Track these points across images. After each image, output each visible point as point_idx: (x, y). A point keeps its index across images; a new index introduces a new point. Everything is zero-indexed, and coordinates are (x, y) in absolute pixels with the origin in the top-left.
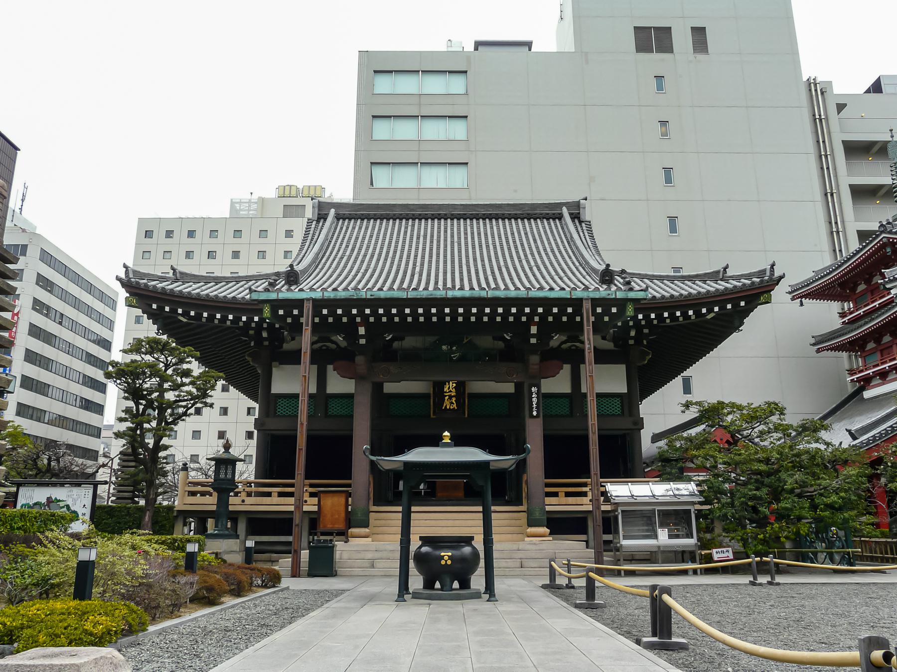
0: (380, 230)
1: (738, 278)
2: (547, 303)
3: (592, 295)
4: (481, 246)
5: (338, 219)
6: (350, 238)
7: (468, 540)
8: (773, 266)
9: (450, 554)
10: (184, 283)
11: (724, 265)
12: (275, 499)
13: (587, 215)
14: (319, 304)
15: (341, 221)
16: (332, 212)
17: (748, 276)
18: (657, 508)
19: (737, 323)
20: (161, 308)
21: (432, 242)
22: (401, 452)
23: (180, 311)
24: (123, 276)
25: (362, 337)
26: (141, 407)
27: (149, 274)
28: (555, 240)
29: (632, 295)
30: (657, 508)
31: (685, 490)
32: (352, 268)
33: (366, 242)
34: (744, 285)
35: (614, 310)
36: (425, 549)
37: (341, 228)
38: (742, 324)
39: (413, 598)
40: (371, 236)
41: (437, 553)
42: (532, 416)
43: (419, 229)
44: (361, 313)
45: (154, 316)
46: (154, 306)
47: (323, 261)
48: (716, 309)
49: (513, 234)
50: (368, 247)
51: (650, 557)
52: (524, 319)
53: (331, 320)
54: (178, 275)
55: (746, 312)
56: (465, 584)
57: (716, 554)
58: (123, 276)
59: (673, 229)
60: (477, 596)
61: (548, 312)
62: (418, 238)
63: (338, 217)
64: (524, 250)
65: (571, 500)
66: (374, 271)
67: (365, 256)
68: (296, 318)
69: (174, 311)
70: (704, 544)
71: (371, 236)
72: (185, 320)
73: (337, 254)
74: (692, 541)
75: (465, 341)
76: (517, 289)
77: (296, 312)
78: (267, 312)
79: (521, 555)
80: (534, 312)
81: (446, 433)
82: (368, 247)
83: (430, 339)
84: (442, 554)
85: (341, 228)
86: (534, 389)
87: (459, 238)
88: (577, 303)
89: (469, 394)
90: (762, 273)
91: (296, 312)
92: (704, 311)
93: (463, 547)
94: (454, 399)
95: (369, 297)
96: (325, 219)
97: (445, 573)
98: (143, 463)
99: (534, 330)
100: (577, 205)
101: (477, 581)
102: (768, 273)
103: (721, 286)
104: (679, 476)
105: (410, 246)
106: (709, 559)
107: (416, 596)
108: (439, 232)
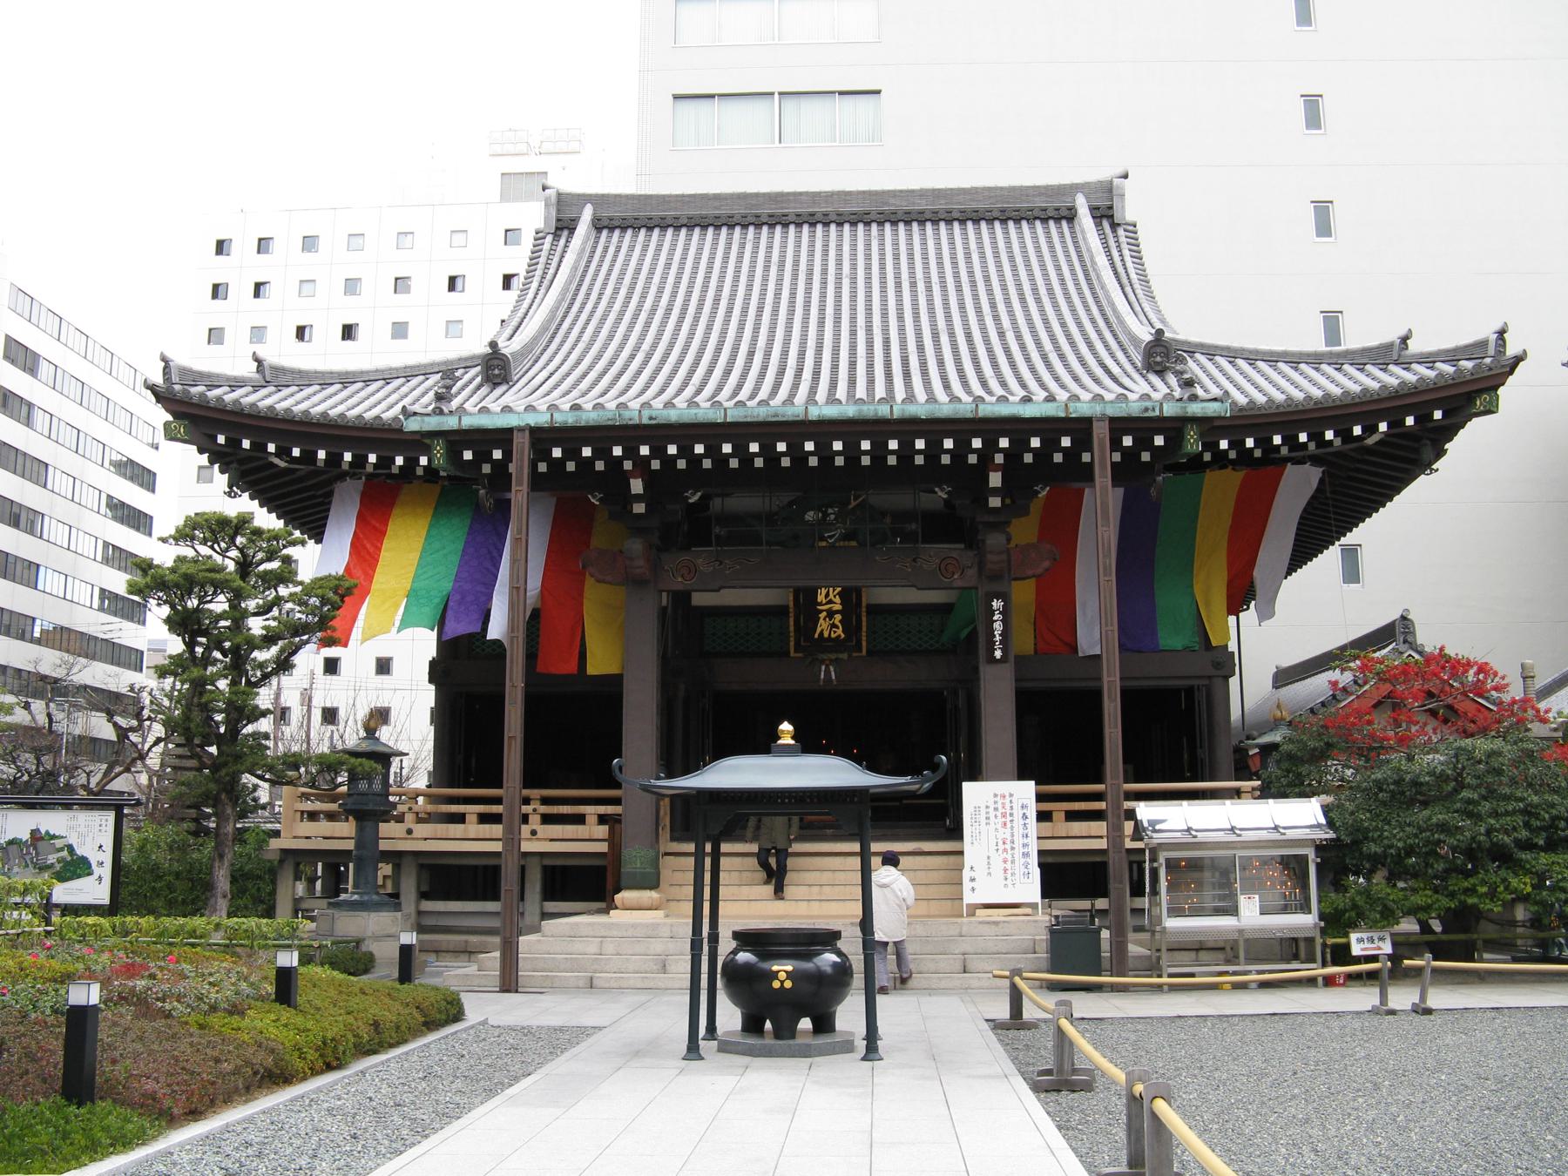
0: (686, 250)
1: (1428, 359)
2: (1019, 427)
3: (1112, 411)
4: (898, 285)
5: (599, 229)
6: (623, 272)
7: (828, 939)
8: (1501, 333)
9: (789, 968)
10: (279, 388)
11: (1403, 332)
12: (472, 828)
13: (1130, 210)
14: (542, 437)
15: (605, 232)
16: (587, 214)
17: (1452, 356)
18: (1240, 853)
19: (1427, 452)
20: (234, 443)
21: (795, 276)
22: (687, 770)
23: (271, 448)
24: (158, 379)
25: (638, 498)
26: (199, 650)
27: (209, 376)
28: (1058, 268)
29: (1195, 409)
30: (1240, 853)
31: (1301, 816)
32: (626, 338)
33: (656, 279)
34: (1441, 375)
35: (1159, 441)
36: (744, 957)
37: (606, 249)
38: (1440, 453)
39: (721, 1050)
40: (668, 266)
41: (765, 965)
42: (992, 660)
43: (770, 247)
44: (631, 452)
45: (222, 458)
46: (221, 439)
47: (566, 325)
48: (1383, 427)
49: (968, 256)
50: (660, 290)
51: (1227, 950)
52: (973, 459)
53: (571, 466)
54: (267, 373)
55: (1449, 430)
56: (824, 1024)
57: (1359, 943)
58: (158, 379)
59: (1324, 227)
60: (847, 1047)
61: (1020, 445)
62: (767, 268)
63: (598, 226)
64: (990, 292)
65: (1078, 827)
66: (671, 345)
67: (653, 311)
68: (501, 468)
69: (259, 447)
70: (1336, 922)
71: (668, 266)
72: (282, 464)
73: (595, 307)
74: (1306, 921)
75: (853, 504)
76: (954, 399)
77: (497, 454)
78: (439, 450)
79: (966, 946)
80: (991, 445)
81: (786, 727)
82: (660, 290)
83: (785, 497)
84: (775, 968)
85: (606, 249)
86: (997, 604)
87: (854, 267)
88: (1080, 427)
89: (868, 606)
90: (1476, 349)
91: (497, 454)
92: (1357, 430)
93: (819, 953)
94: (838, 617)
95: (645, 421)
96: (572, 230)
97: (783, 1000)
98: (215, 739)
99: (995, 480)
100: (1108, 189)
101: (849, 1015)
102: (1491, 351)
103: (1395, 377)
104: (1293, 787)
105: (749, 287)
106: (1341, 955)
107: (726, 1047)
108: (811, 253)
